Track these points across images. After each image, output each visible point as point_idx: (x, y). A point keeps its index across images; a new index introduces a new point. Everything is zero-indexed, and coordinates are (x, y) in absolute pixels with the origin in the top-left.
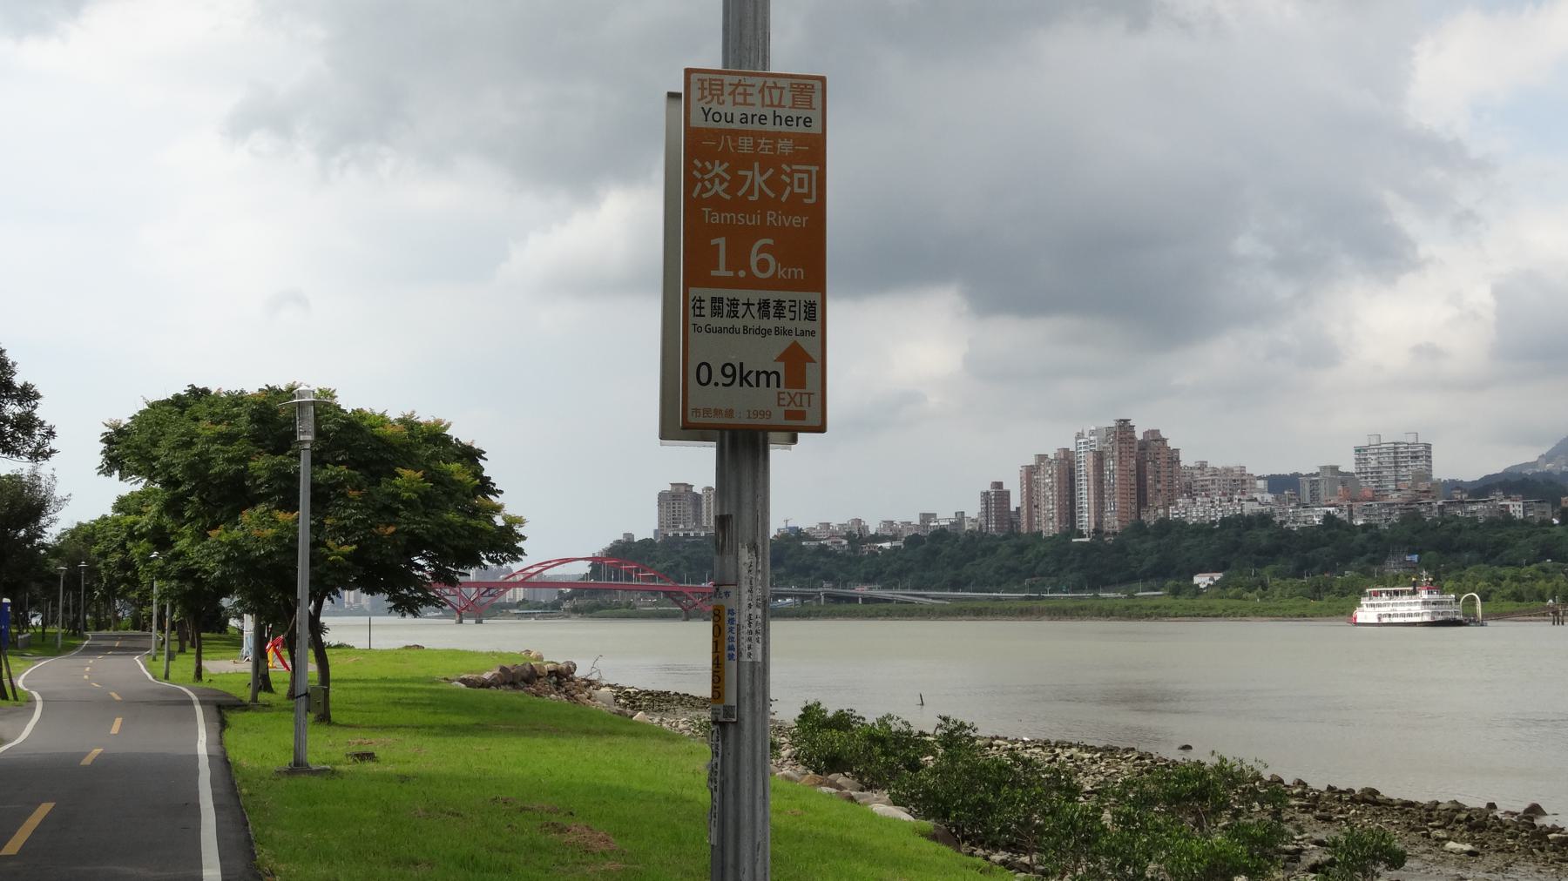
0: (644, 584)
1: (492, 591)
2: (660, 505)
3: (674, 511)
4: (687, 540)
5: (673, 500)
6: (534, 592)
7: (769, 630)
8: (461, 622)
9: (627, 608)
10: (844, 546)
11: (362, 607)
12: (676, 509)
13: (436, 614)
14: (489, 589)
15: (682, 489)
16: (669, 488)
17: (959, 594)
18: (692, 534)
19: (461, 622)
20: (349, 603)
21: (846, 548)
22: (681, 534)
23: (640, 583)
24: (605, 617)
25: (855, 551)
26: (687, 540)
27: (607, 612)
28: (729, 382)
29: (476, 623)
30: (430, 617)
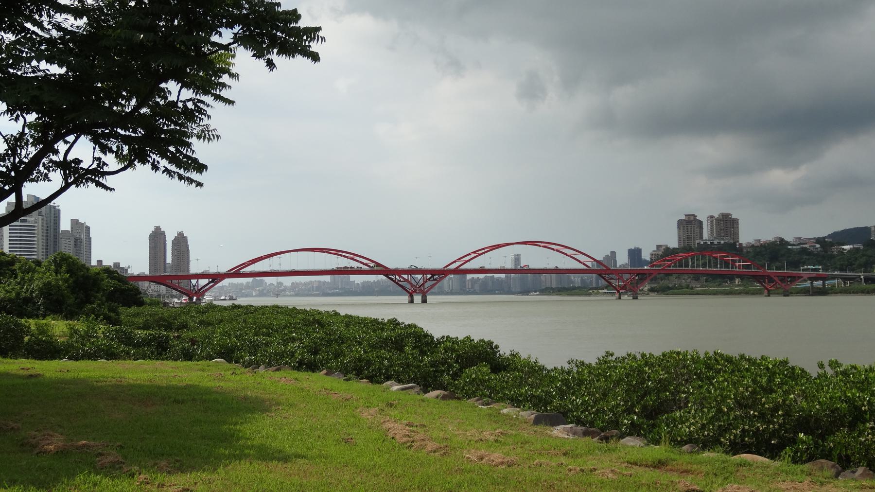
0: (745, 270)
1: (435, 277)
2: (678, 228)
3: (687, 231)
4: (713, 246)
5: (687, 224)
6: (551, 277)
7: (726, 296)
8: (620, 298)
9: (687, 288)
10: (817, 248)
11: (475, 290)
12: (689, 230)
13: (535, 293)
14: (433, 276)
15: (692, 218)
16: (684, 217)
17: (848, 274)
18: (716, 243)
19: (620, 298)
20: (469, 289)
21: (820, 249)
22: (709, 243)
23: (756, 270)
24: (673, 294)
25: (826, 252)
26: (713, 246)
27: (676, 291)
28: (23, 119)
29: (633, 299)
30: (531, 295)
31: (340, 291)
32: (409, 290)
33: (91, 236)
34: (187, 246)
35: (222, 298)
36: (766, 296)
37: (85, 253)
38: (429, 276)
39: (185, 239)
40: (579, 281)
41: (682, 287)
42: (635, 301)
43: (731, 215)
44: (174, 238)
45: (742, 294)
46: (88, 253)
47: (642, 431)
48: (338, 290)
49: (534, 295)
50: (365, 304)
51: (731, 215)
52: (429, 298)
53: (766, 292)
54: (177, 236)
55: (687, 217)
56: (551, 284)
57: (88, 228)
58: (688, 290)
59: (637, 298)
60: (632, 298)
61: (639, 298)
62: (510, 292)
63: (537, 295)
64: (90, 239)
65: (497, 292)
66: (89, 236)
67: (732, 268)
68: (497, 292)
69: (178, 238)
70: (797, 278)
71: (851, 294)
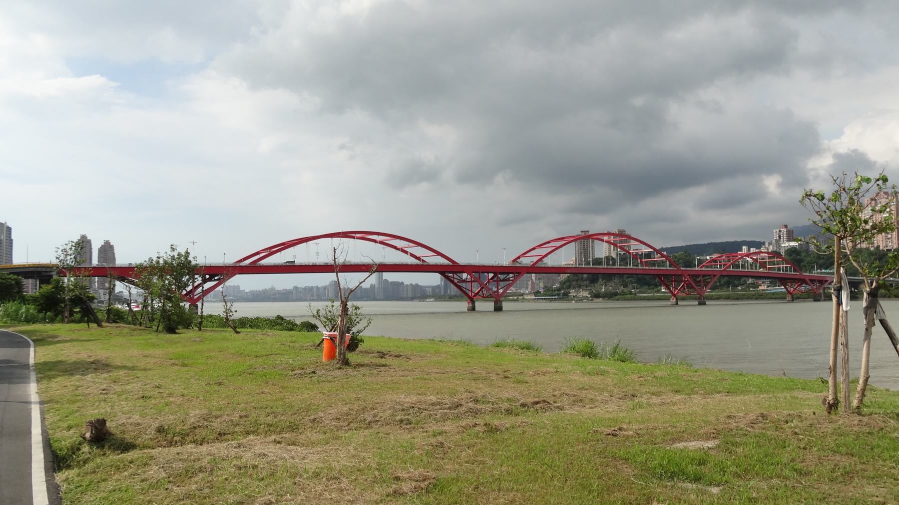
12: (585, 244)
29: (700, 304)
31: (234, 299)
32: (467, 291)
33: (12, 238)
34: (113, 254)
35: (585, 276)
36: (789, 301)
37: (5, 255)
38: (491, 275)
39: (112, 247)
40: (430, 291)
41: (625, 293)
42: (703, 308)
43: (625, 231)
44: (101, 246)
45: (721, 299)
46: (8, 253)
47: (75, 310)
48: (231, 298)
49: (430, 301)
50: (608, 308)
51: (625, 231)
52: (506, 305)
53: (789, 298)
54: (103, 244)
55: (583, 234)
56: (407, 294)
57: (9, 230)
58: (632, 296)
59: (704, 304)
60: (696, 303)
61: (707, 303)
62: (375, 299)
63: (434, 301)
64: (12, 240)
65: (751, 289)
66: (10, 237)
67: (787, 267)
68: (751, 289)
69: (105, 246)
70: (824, 282)
71: (892, 299)
